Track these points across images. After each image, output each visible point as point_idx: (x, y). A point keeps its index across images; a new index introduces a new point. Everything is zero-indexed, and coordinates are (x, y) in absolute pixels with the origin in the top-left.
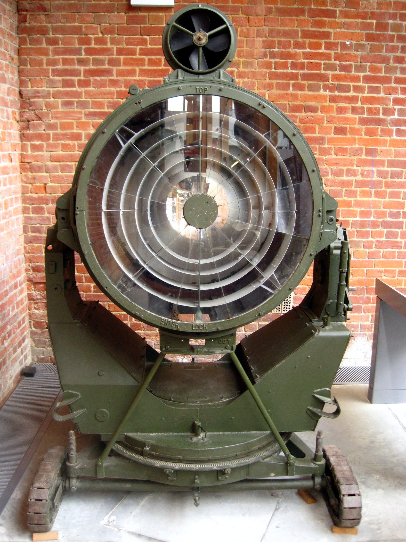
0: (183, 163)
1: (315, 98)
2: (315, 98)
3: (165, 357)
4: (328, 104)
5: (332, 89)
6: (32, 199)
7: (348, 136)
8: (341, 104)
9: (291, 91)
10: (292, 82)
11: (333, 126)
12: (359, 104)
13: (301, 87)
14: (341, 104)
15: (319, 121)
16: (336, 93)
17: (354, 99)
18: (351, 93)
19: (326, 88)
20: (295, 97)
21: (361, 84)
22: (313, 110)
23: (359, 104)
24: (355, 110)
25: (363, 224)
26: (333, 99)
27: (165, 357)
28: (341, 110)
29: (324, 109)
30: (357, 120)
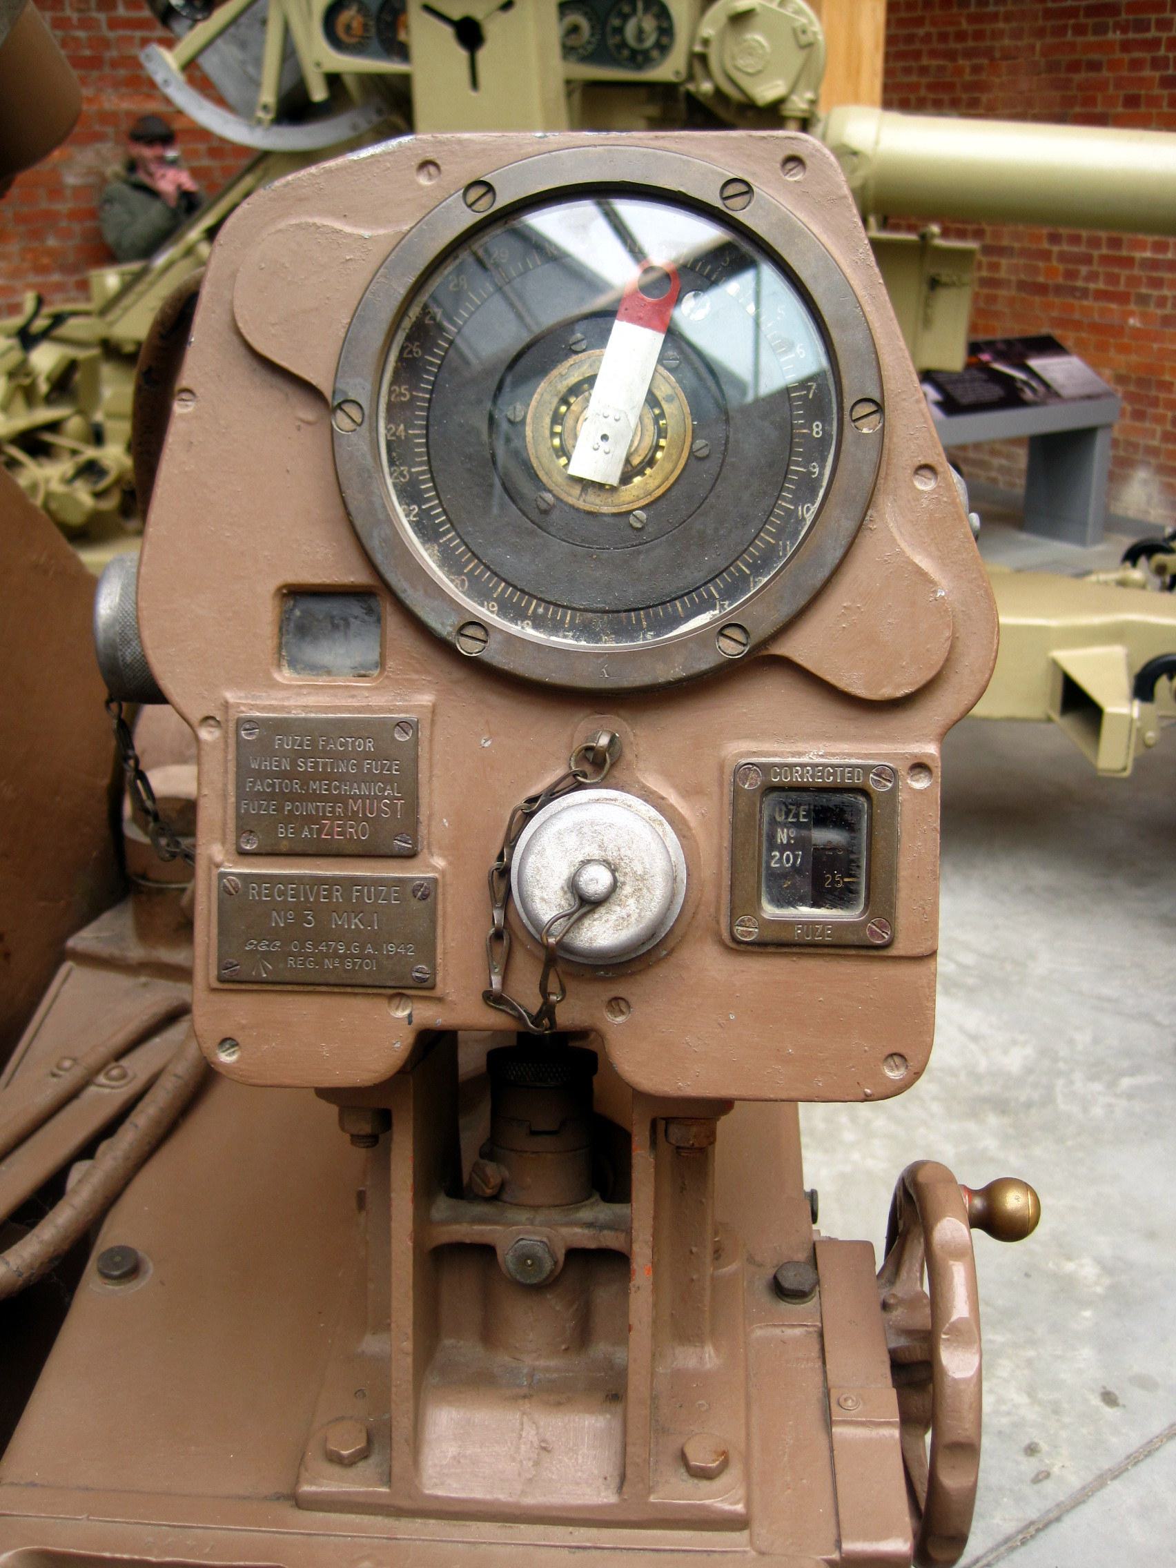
0: (625, 1251)
1: (1100, 47)
2: (1100, 47)
3: (812, 1117)
4: (1118, 55)
5: (1124, 30)
6: (261, 775)
7: (1143, 109)
8: (1137, 55)
9: (1069, 36)
10: (1072, 22)
11: (1122, 93)
12: (1162, 52)
13: (1080, 30)
14: (1137, 55)
15: (1102, 86)
16: (1131, 35)
17: (1155, 44)
18: (1153, 33)
19: (1117, 26)
20: (1072, 46)
21: (1082, 20)
22: (1094, 66)
23: (1162, 52)
24: (1156, 64)
25: (1154, 265)
26: (1126, 46)
27: (812, 1117)
28: (1136, 65)
29: (1113, 65)
30: (1157, 81)
